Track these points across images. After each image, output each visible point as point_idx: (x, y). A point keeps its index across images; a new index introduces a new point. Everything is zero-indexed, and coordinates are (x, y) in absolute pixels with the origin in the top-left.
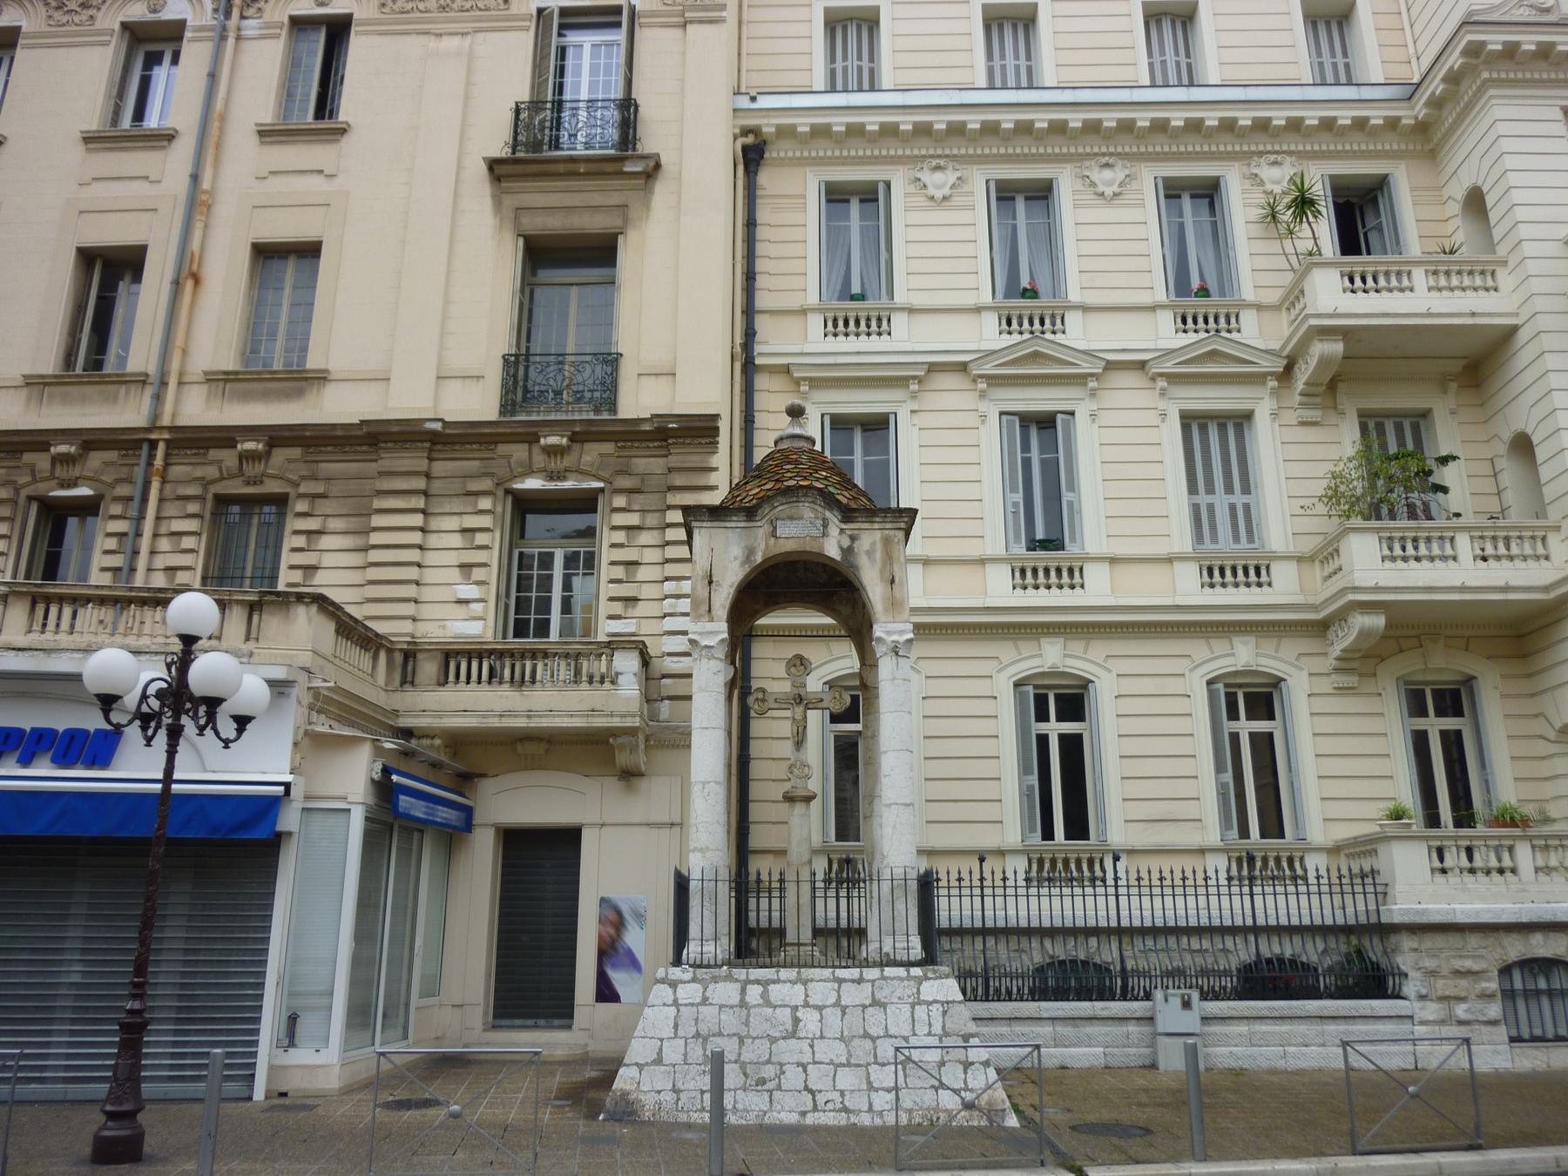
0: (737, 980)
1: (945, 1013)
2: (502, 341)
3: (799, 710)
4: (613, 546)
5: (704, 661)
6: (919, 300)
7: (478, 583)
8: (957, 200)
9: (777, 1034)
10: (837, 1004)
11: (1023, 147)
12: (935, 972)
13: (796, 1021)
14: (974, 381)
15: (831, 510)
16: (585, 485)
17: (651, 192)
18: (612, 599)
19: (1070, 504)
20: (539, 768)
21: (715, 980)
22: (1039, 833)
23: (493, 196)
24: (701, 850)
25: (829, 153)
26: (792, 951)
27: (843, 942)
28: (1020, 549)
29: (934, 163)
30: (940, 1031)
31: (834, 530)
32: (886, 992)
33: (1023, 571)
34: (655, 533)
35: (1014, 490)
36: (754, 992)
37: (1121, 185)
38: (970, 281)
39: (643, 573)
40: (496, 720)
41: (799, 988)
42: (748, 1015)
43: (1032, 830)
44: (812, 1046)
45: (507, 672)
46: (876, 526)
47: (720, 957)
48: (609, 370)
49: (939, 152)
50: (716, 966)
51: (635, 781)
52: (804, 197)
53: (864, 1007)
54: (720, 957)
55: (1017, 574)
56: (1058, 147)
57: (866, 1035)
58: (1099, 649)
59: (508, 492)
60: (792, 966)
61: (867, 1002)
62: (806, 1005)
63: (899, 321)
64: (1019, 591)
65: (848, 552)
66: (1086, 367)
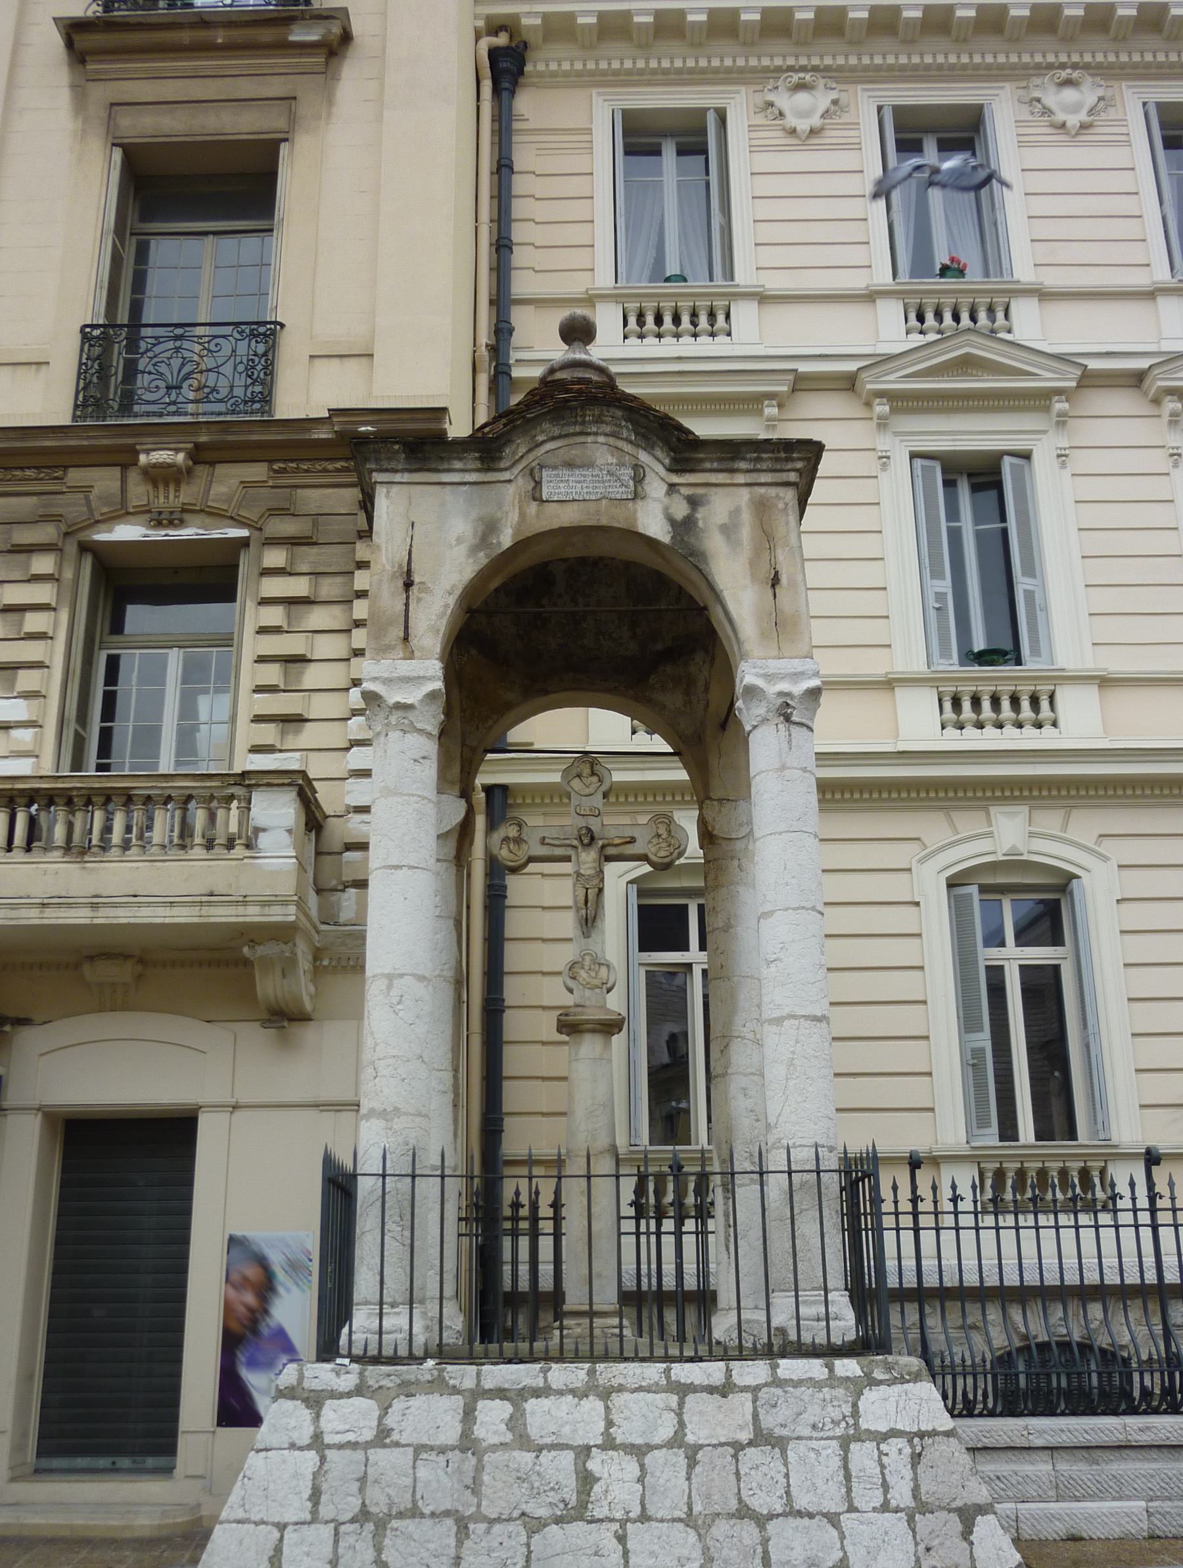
0: (455, 1391)
1: (916, 1458)
2: (83, 303)
3: (588, 858)
4: (263, 631)
5: (395, 735)
6: (775, 283)
7: (28, 695)
8: (831, 136)
9: (543, 1512)
10: (677, 1441)
11: (935, 53)
12: (889, 1368)
13: (587, 1480)
14: (868, 405)
15: (649, 448)
16: (216, 534)
17: (336, 78)
18: (258, 719)
19: (1029, 595)
20: (126, 1007)
21: (407, 1389)
22: (994, 1129)
23: (73, 87)
24: (383, 1115)
25: (628, 64)
26: (576, 1328)
27: (671, 1315)
28: (951, 665)
29: (795, 78)
30: (907, 1501)
31: (656, 487)
32: (784, 1413)
33: (957, 703)
34: (336, 610)
35: (937, 574)
36: (493, 1416)
37: (1091, 112)
38: (856, 255)
39: (313, 676)
40: (34, 913)
41: (593, 1406)
42: (479, 1468)
43: (983, 1123)
44: (622, 1539)
45: (59, 832)
46: (741, 478)
47: (420, 1339)
48: (261, 349)
49: (803, 61)
50: (413, 1359)
51: (295, 1029)
52: (589, 131)
53: (738, 1447)
54: (420, 1339)
55: (948, 705)
56: (991, 53)
57: (744, 1512)
58: (1086, 825)
59: (85, 548)
60: (577, 1358)
61: (745, 1436)
62: (609, 1444)
63: (744, 315)
64: (951, 732)
65: (684, 527)
66: (1047, 379)
